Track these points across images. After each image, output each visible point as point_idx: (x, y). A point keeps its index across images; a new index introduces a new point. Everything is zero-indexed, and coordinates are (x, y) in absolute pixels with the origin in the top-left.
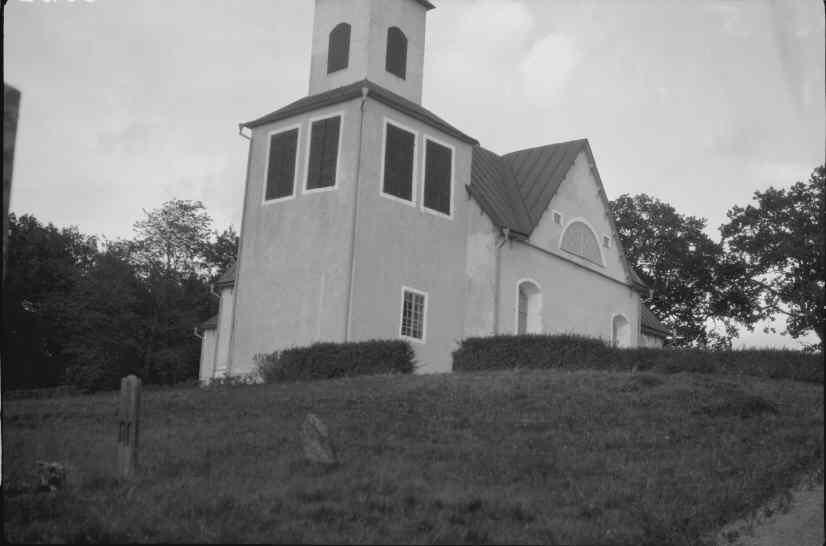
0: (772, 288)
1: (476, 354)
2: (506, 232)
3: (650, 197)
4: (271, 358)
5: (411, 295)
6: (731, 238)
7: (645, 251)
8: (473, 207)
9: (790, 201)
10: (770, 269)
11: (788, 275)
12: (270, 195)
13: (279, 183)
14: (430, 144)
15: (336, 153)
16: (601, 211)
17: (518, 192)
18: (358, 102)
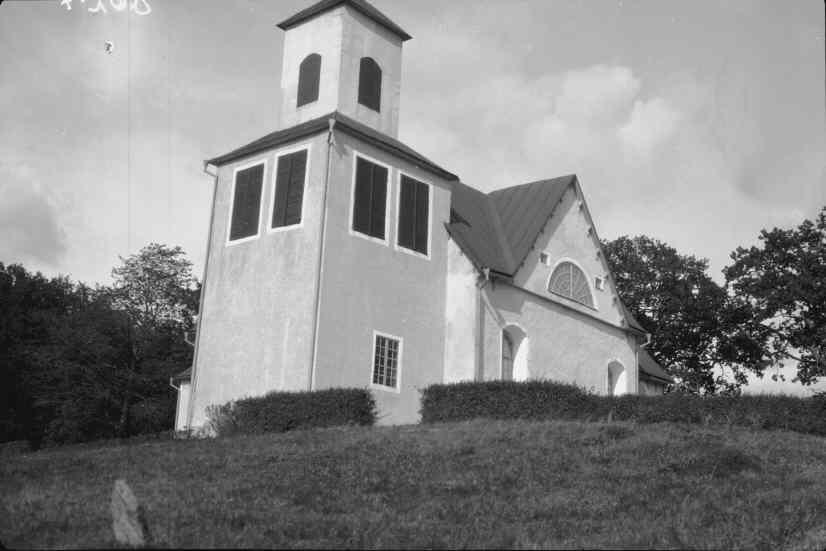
0: (781, 332)
1: (441, 401)
2: (487, 271)
3: (650, 238)
4: (225, 409)
5: (384, 339)
6: (735, 282)
7: (646, 295)
8: (452, 247)
9: (795, 242)
10: (778, 313)
11: (797, 320)
12: (235, 235)
13: (244, 223)
14: (404, 179)
15: (301, 188)
16: (592, 251)
17: (501, 236)
18: (324, 137)
